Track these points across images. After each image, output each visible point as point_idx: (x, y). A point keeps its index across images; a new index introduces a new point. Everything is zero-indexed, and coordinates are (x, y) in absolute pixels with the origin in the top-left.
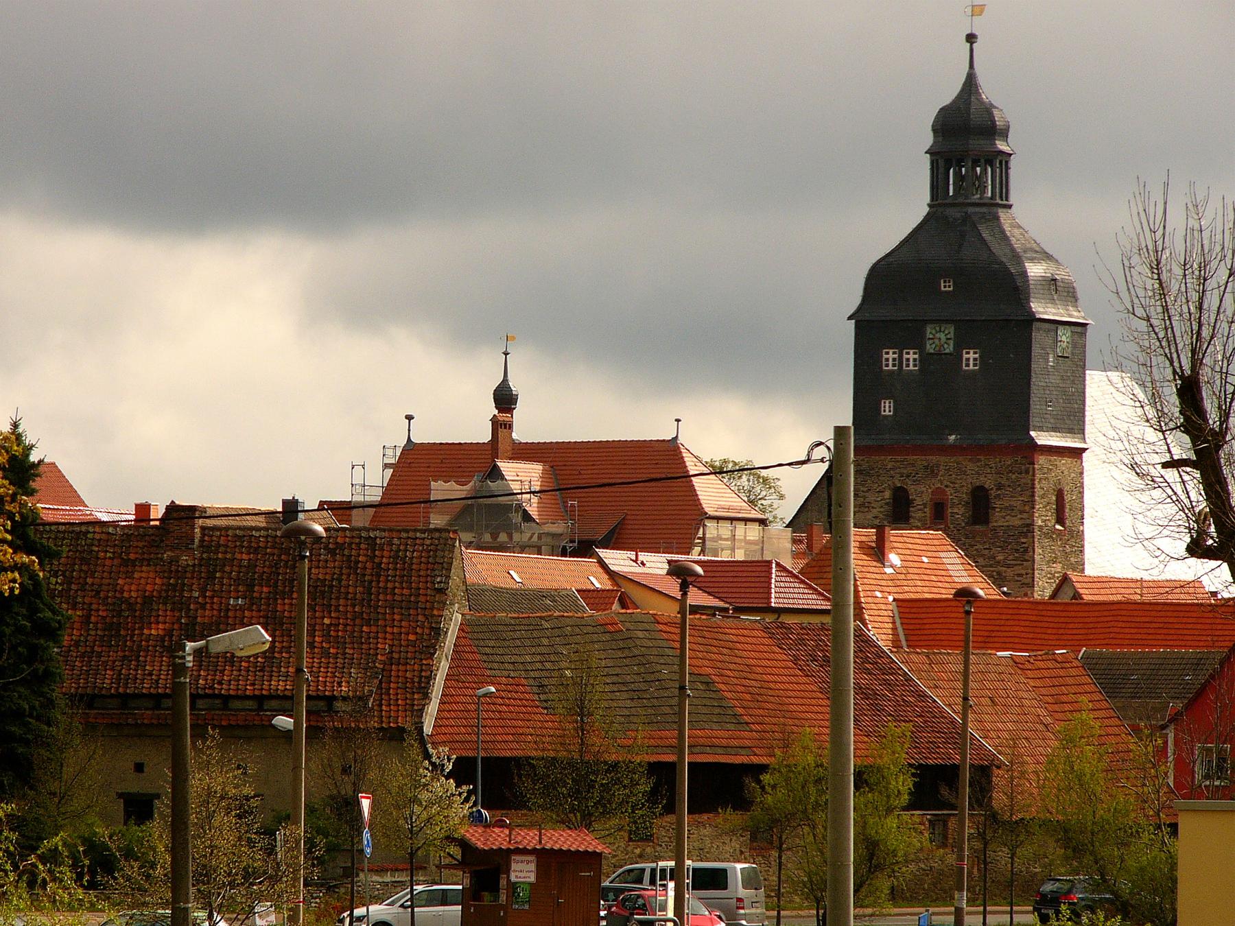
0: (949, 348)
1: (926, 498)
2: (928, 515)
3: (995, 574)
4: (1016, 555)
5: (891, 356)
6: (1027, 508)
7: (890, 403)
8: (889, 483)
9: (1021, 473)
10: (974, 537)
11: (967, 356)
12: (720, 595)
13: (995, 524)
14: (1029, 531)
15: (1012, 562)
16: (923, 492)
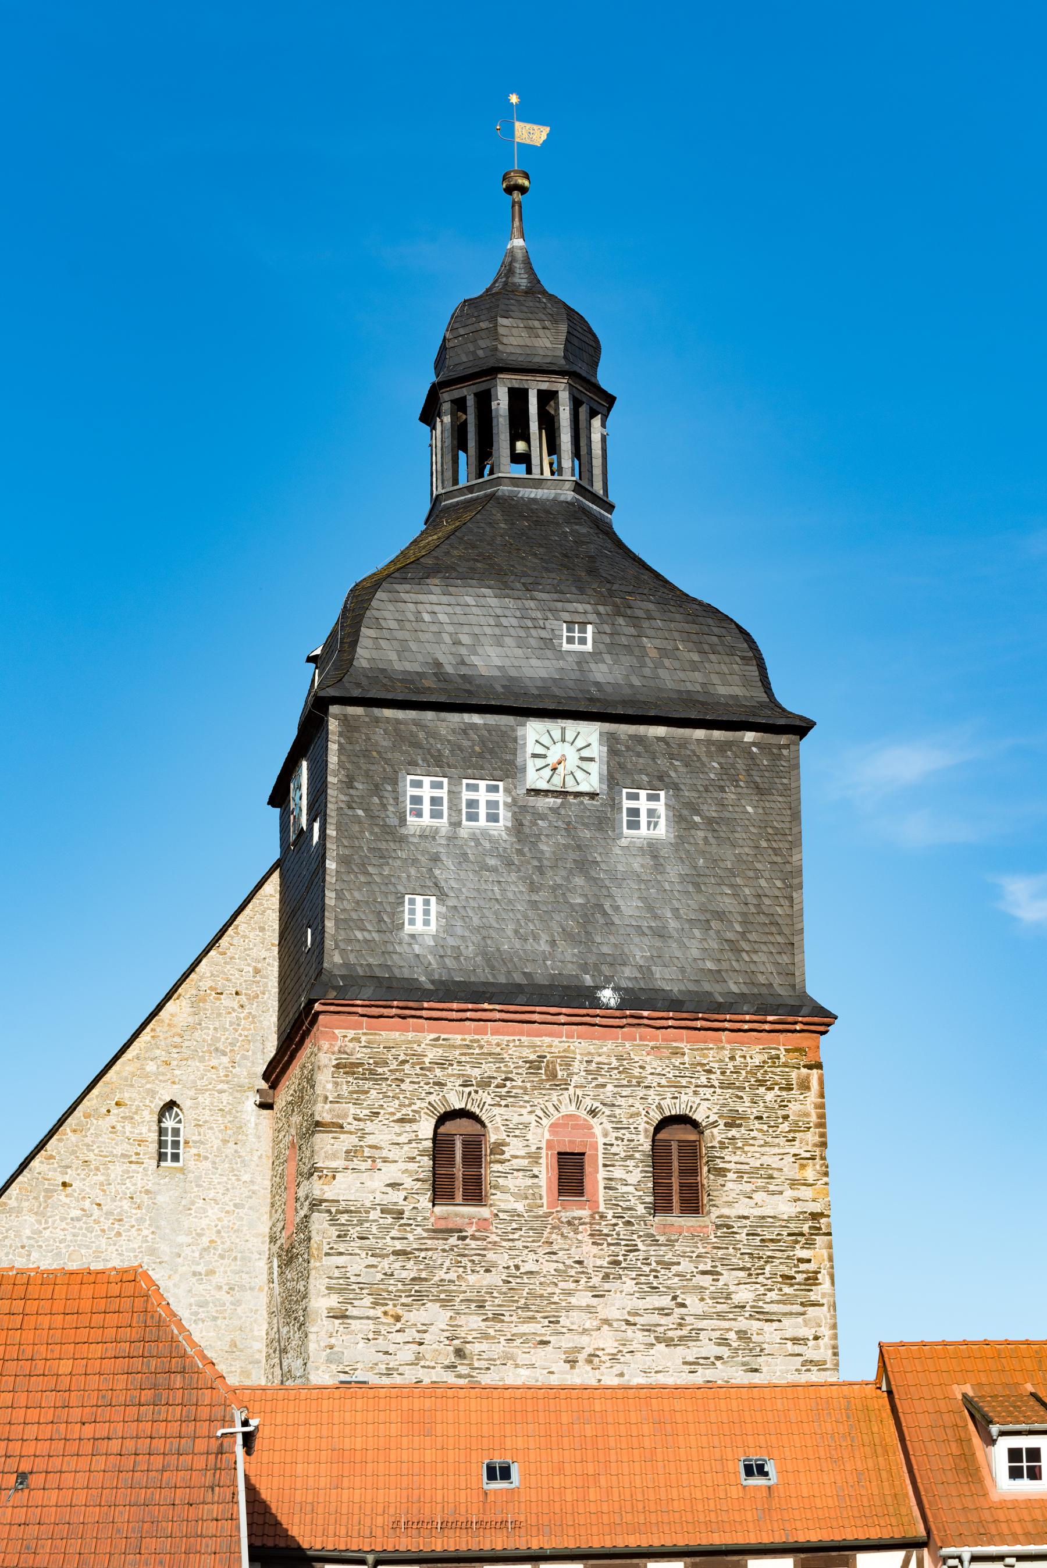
0: (591, 781)
1: (540, 1136)
2: (543, 1181)
3: (732, 1335)
4: (787, 1290)
5: (426, 792)
6: (810, 1174)
7: (427, 903)
8: (432, 1098)
9: (789, 1088)
10: (670, 1243)
11: (633, 804)
12: (590, 336)
13: (726, 1211)
14: (816, 1230)
15: (774, 1308)
16: (526, 1126)
